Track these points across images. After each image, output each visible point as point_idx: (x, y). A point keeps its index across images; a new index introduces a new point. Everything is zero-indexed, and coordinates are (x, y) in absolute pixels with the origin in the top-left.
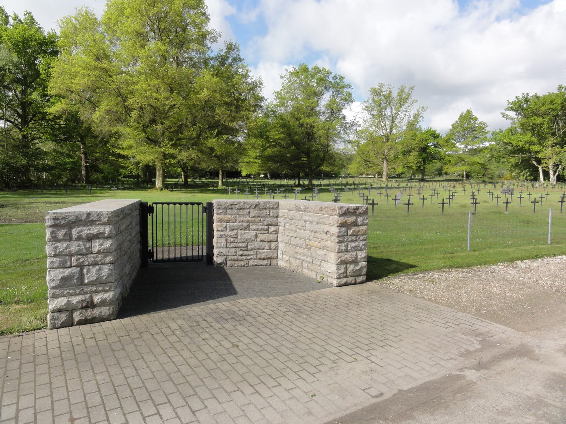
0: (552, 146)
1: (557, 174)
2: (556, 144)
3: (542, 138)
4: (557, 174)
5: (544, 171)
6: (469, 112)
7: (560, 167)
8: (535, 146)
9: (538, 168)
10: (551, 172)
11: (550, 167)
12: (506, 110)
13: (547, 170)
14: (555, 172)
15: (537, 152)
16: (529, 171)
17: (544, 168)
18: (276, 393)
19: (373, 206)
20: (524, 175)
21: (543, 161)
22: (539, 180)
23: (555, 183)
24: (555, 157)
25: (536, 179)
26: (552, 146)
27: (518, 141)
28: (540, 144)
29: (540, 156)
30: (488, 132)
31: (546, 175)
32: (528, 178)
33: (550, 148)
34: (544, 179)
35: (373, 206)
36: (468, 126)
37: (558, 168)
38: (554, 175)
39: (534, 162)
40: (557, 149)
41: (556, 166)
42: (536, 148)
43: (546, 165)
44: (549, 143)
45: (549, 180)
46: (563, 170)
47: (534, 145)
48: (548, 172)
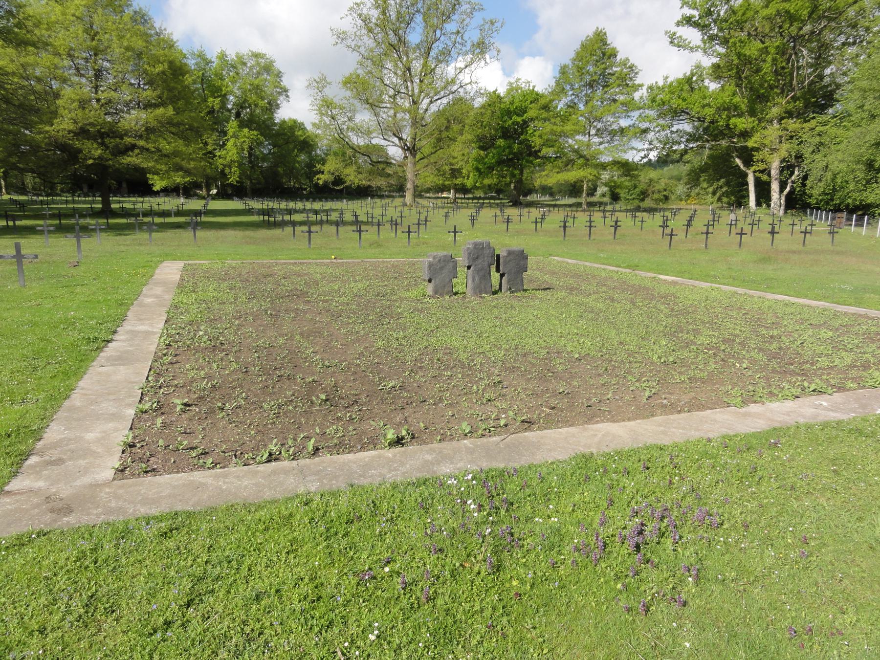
0: (780, 120)
1: (788, 189)
2: (790, 114)
3: (759, 99)
4: (788, 189)
5: (758, 183)
6: (600, 38)
7: (796, 173)
8: (743, 120)
9: (746, 175)
10: (775, 186)
11: (773, 172)
12: (678, 24)
13: (765, 178)
14: (783, 186)
15: (745, 134)
16: (727, 184)
17: (757, 174)
18: (681, 165)
19: (310, 235)
20: (714, 193)
21: (757, 156)
22: (746, 204)
23: (782, 212)
24: (786, 146)
25: (740, 201)
26: (780, 120)
27: (703, 107)
28: (752, 113)
29: (751, 144)
30: (641, 85)
31: (764, 195)
32: (725, 199)
33: (776, 125)
34: (758, 204)
35: (310, 235)
36: (598, 66)
37: (792, 173)
38: (781, 191)
39: (738, 161)
40: (792, 124)
41: (787, 168)
42: (742, 123)
43: (762, 166)
44: (775, 111)
45: (769, 206)
46: (805, 178)
47: (740, 115)
48: (768, 184)
